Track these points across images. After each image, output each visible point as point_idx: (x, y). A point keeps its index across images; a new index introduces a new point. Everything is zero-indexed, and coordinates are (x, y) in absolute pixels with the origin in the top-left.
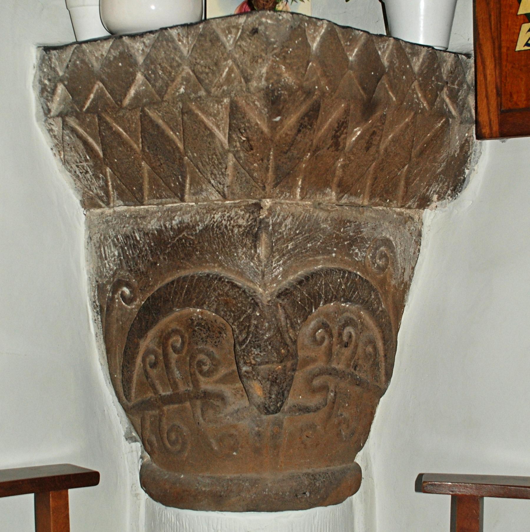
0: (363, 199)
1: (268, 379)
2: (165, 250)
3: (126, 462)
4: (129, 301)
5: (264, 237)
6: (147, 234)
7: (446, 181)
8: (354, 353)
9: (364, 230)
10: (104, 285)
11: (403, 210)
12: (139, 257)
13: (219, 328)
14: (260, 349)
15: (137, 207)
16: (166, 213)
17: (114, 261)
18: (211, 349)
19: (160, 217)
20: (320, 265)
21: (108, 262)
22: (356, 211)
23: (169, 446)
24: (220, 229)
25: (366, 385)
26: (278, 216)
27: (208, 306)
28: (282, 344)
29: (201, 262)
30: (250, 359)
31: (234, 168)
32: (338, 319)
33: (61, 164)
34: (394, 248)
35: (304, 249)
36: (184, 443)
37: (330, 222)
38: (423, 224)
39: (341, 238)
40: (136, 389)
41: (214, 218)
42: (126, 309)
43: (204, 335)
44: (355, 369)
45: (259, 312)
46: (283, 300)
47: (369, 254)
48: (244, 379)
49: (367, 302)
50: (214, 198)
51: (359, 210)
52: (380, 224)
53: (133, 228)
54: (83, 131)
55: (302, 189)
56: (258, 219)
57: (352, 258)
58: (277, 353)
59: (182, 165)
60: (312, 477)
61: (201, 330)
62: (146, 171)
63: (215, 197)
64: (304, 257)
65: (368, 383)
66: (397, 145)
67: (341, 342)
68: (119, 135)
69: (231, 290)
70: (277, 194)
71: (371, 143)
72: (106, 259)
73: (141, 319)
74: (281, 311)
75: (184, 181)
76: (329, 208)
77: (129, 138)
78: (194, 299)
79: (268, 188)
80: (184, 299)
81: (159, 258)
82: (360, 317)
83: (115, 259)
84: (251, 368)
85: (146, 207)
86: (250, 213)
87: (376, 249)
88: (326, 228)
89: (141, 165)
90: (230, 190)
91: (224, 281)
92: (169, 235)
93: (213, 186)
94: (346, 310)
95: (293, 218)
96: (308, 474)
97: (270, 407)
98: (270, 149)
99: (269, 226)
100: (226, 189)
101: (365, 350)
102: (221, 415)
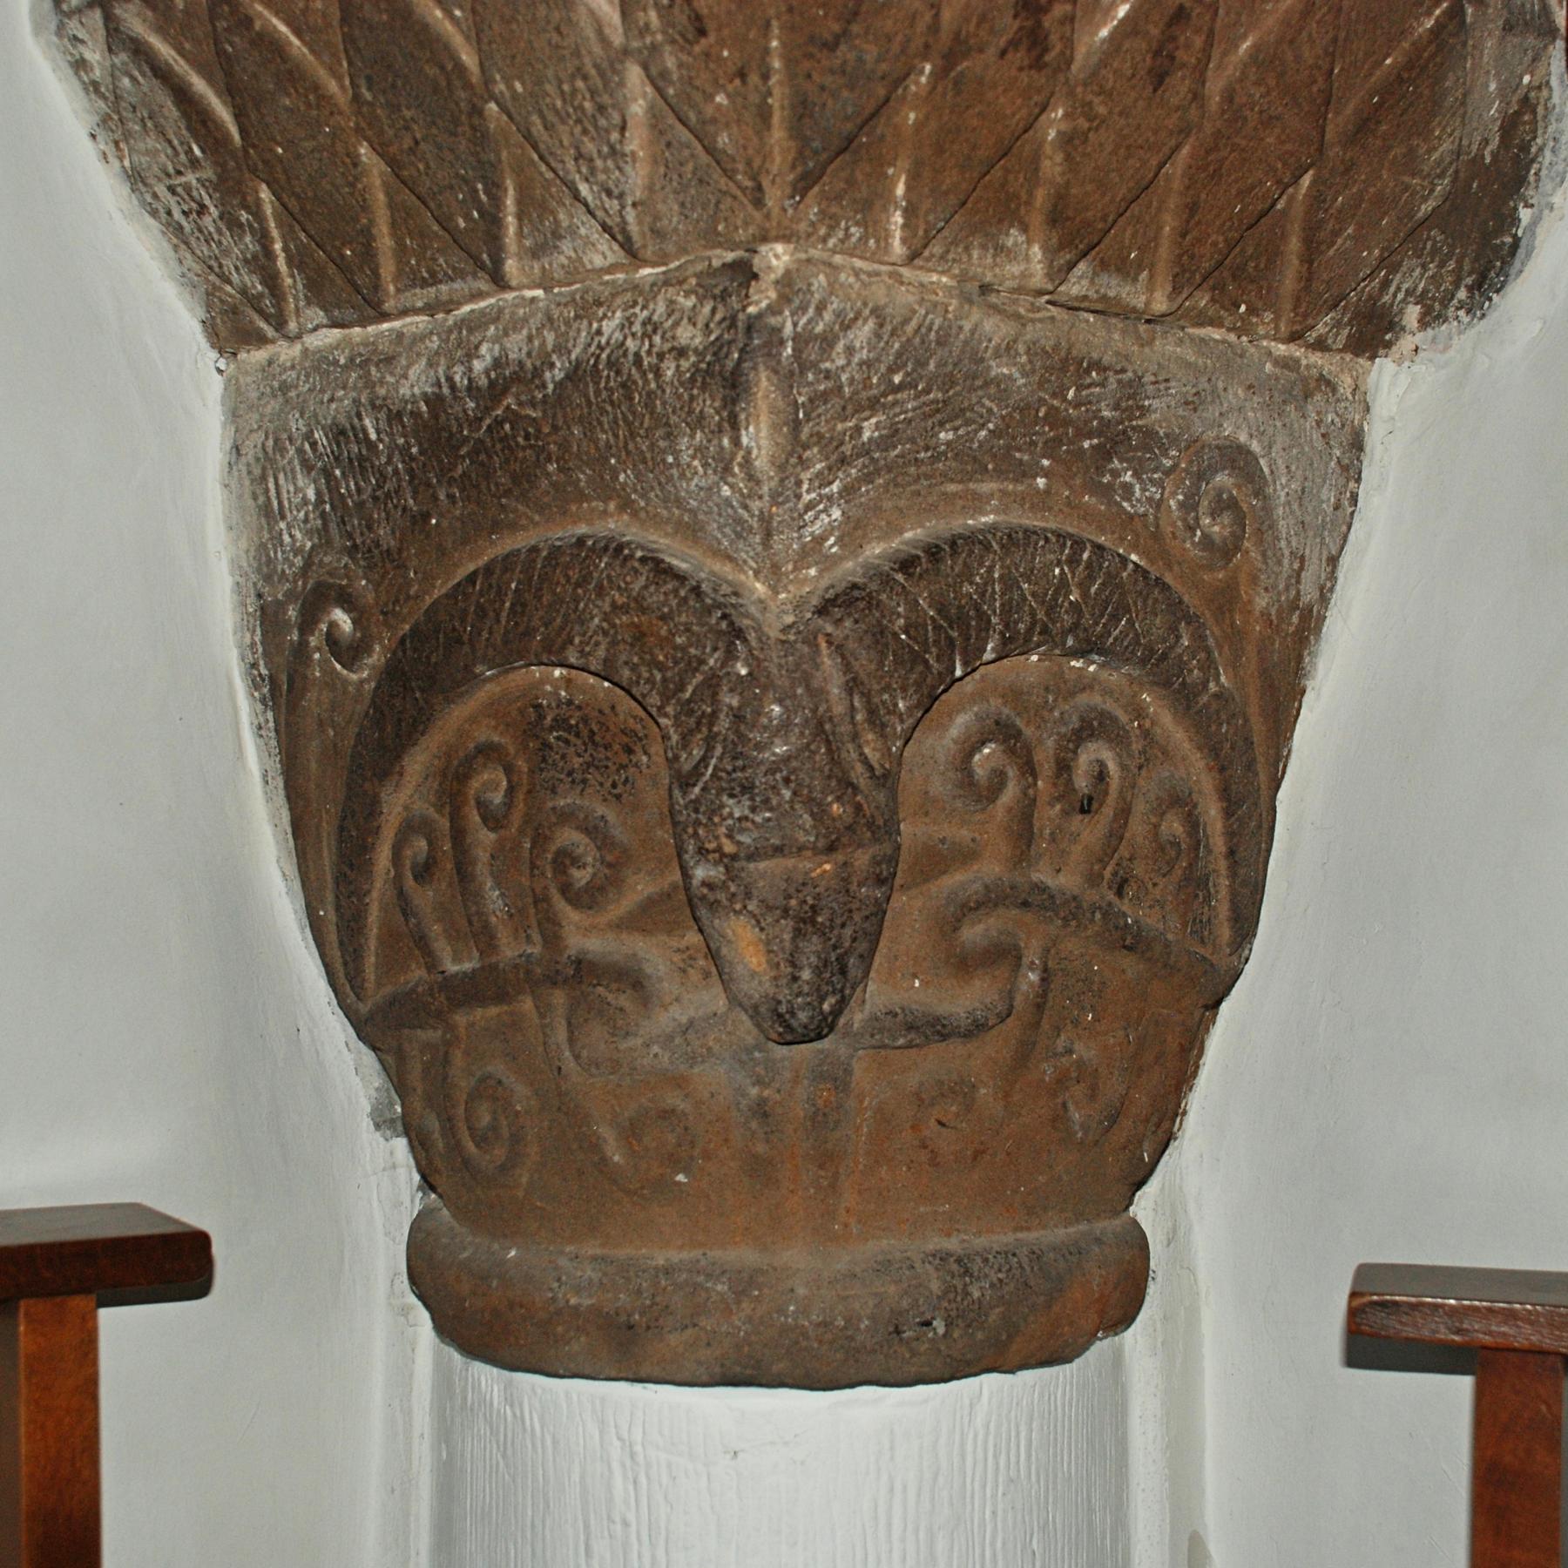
0: (1150, 289)
1: (786, 911)
2: (453, 467)
3: (375, 1204)
4: (350, 653)
5: (764, 384)
6: (399, 415)
7: (1450, 256)
8: (1116, 836)
9: (1156, 403)
10: (281, 606)
11: (1297, 351)
12: (375, 499)
13: (622, 731)
14: (752, 799)
15: (370, 329)
16: (453, 337)
17: (306, 521)
18: (601, 810)
19: (437, 353)
20: (986, 514)
21: (289, 527)
22: (1124, 332)
23: (471, 1147)
24: (618, 373)
25: (1158, 948)
26: (820, 309)
27: (582, 651)
28: (834, 783)
29: (566, 498)
30: (717, 838)
31: (653, 127)
32: (1056, 714)
33: (125, 189)
34: (1266, 481)
35: (927, 449)
36: (516, 1139)
37: (1024, 359)
38: (1368, 409)
39: (1067, 422)
40: (377, 955)
41: (599, 332)
42: (345, 682)
43: (577, 762)
44: (1120, 893)
45: (747, 664)
46: (838, 622)
47: (1174, 494)
48: (703, 912)
49: (1164, 657)
50: (598, 261)
51: (1136, 331)
52: (1214, 391)
53: (356, 402)
54: (173, 53)
55: (909, 213)
56: (741, 316)
57: (1111, 503)
58: (812, 814)
59: (481, 137)
60: (955, 1267)
61: (567, 742)
62: (378, 182)
63: (603, 253)
64: (927, 477)
65: (1167, 945)
66: (1272, 82)
67: (1065, 791)
68: (271, 46)
69: (652, 589)
70: (813, 224)
71: (1172, 58)
72: (283, 517)
73: (382, 713)
74: (828, 661)
75: (497, 201)
76: (1022, 311)
77: (311, 58)
78: (536, 630)
79: (774, 196)
80: (507, 632)
81: (435, 498)
82: (1139, 712)
83: (307, 514)
84: (722, 869)
85: (397, 324)
86: (714, 298)
87: (1201, 476)
88: (1010, 377)
89: (359, 155)
90: (648, 219)
91: (631, 556)
92: (465, 411)
93: (586, 205)
94: (1085, 684)
95: (881, 326)
96: (943, 1257)
97: (793, 1014)
98: (768, 25)
99: (782, 343)
100: (631, 215)
101: (1156, 826)
102: (632, 1042)
